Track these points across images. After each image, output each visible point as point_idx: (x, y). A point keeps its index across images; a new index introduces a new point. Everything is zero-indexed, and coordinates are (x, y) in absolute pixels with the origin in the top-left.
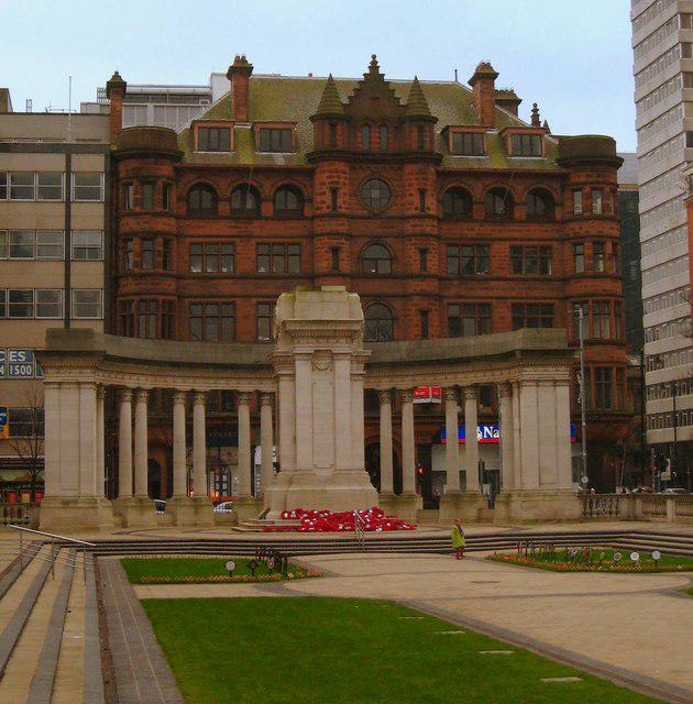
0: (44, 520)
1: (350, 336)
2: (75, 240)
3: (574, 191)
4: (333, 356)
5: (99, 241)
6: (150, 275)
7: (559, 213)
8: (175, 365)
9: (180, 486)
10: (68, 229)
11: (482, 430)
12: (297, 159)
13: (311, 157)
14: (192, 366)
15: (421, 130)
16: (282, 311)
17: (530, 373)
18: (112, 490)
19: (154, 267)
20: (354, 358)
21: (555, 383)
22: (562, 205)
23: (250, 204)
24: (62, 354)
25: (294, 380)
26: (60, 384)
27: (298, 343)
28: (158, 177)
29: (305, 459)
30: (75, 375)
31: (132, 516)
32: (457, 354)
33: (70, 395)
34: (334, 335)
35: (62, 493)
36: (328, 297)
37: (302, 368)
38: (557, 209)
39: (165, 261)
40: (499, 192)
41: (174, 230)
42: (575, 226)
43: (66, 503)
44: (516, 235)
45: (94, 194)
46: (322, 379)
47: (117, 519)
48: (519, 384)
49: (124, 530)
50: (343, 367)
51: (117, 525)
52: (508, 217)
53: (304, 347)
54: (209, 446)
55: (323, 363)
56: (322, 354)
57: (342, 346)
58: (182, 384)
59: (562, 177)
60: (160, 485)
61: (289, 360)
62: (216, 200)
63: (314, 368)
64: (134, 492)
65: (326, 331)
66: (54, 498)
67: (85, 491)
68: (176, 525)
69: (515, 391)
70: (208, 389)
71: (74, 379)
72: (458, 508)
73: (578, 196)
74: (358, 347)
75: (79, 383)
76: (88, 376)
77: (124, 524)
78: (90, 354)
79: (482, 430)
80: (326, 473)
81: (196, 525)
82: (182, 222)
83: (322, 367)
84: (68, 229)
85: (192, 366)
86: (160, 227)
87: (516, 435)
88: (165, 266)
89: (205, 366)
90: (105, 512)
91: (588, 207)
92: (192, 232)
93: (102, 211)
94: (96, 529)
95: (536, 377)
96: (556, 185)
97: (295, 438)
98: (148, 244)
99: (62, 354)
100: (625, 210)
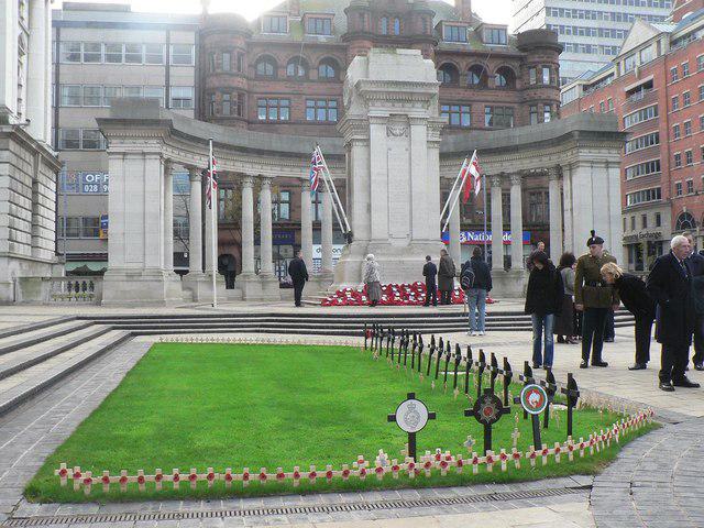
0: (108, 294)
1: (427, 100)
2: (174, 93)
3: (530, 68)
4: (409, 121)
5: (190, 93)
6: (229, 119)
7: (518, 85)
8: (244, 150)
9: (249, 263)
10: (168, 87)
11: (466, 235)
12: (334, 39)
13: (345, 38)
14: (260, 152)
15: (424, 20)
16: (355, 72)
17: (585, 154)
18: (181, 260)
19: (231, 113)
20: (431, 125)
21: (608, 164)
22: (520, 78)
23: (301, 72)
24: (125, 123)
25: (368, 146)
26: (124, 154)
27: (373, 105)
28: (235, 48)
29: (379, 230)
30: (140, 146)
31: (201, 290)
32: (504, 144)
33: (134, 166)
34: (409, 99)
35: (125, 266)
36: (403, 60)
37: (377, 132)
38: (518, 82)
39: (239, 109)
40: (476, 69)
41: (246, 88)
42: (532, 92)
43: (131, 276)
44: (489, 98)
45: (187, 61)
46: (398, 144)
47: (188, 293)
48: (572, 167)
49: (193, 304)
50: (420, 132)
51: (185, 300)
52: (483, 85)
53: (378, 110)
54: (275, 243)
55: (398, 129)
56: (397, 119)
57: (417, 111)
58: (251, 169)
59: (521, 59)
60: (229, 268)
61: (363, 125)
62: (276, 67)
63: (389, 133)
64: (204, 268)
65: (403, 94)
66: (118, 270)
67: (149, 263)
68: (243, 300)
69: (566, 174)
70: (274, 175)
71: (138, 149)
72: (504, 284)
73: (533, 71)
74: (431, 112)
75: (144, 154)
76: (154, 146)
77: (194, 299)
78: (157, 122)
79: (466, 235)
80: (404, 243)
81: (262, 300)
82: (252, 83)
83: (398, 132)
84: (168, 87)
85: (260, 152)
86: (235, 84)
87: (567, 215)
88: (239, 114)
89: (272, 153)
90: (172, 284)
91: (540, 79)
92: (258, 90)
93: (193, 74)
94: (161, 303)
95: (591, 158)
96: (517, 64)
97: (369, 206)
98: (226, 97)
99: (125, 123)
100: (524, 122)
